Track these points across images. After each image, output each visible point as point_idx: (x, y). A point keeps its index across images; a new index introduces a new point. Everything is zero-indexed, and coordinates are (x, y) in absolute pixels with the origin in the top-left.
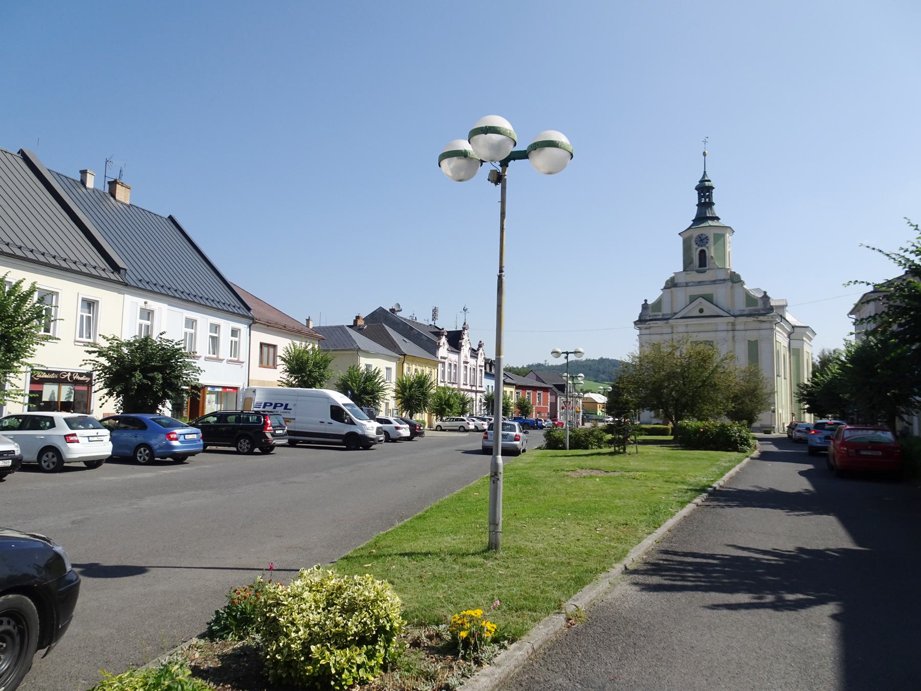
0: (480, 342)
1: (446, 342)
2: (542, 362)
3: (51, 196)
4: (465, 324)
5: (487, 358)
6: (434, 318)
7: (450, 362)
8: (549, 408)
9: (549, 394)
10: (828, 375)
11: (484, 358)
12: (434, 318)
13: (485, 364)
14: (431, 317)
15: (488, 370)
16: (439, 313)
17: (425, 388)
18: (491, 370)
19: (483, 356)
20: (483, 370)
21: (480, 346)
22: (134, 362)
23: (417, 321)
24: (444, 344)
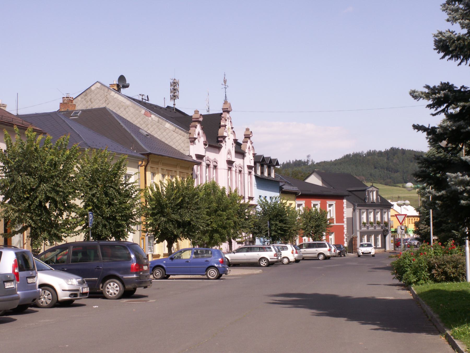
0: (247, 129)
1: (201, 132)
2: (304, 159)
3: (130, 299)
4: (226, 102)
5: (258, 154)
6: (174, 97)
7: (208, 162)
8: (345, 226)
9: (345, 201)
10: (77, 167)
11: (254, 155)
12: (174, 97)
13: (255, 163)
14: (168, 94)
15: (259, 173)
16: (180, 88)
17: (327, 229)
18: (262, 173)
19: (252, 152)
20: (253, 173)
21: (247, 137)
22: (10, 164)
23: (150, 102)
24: (199, 134)
